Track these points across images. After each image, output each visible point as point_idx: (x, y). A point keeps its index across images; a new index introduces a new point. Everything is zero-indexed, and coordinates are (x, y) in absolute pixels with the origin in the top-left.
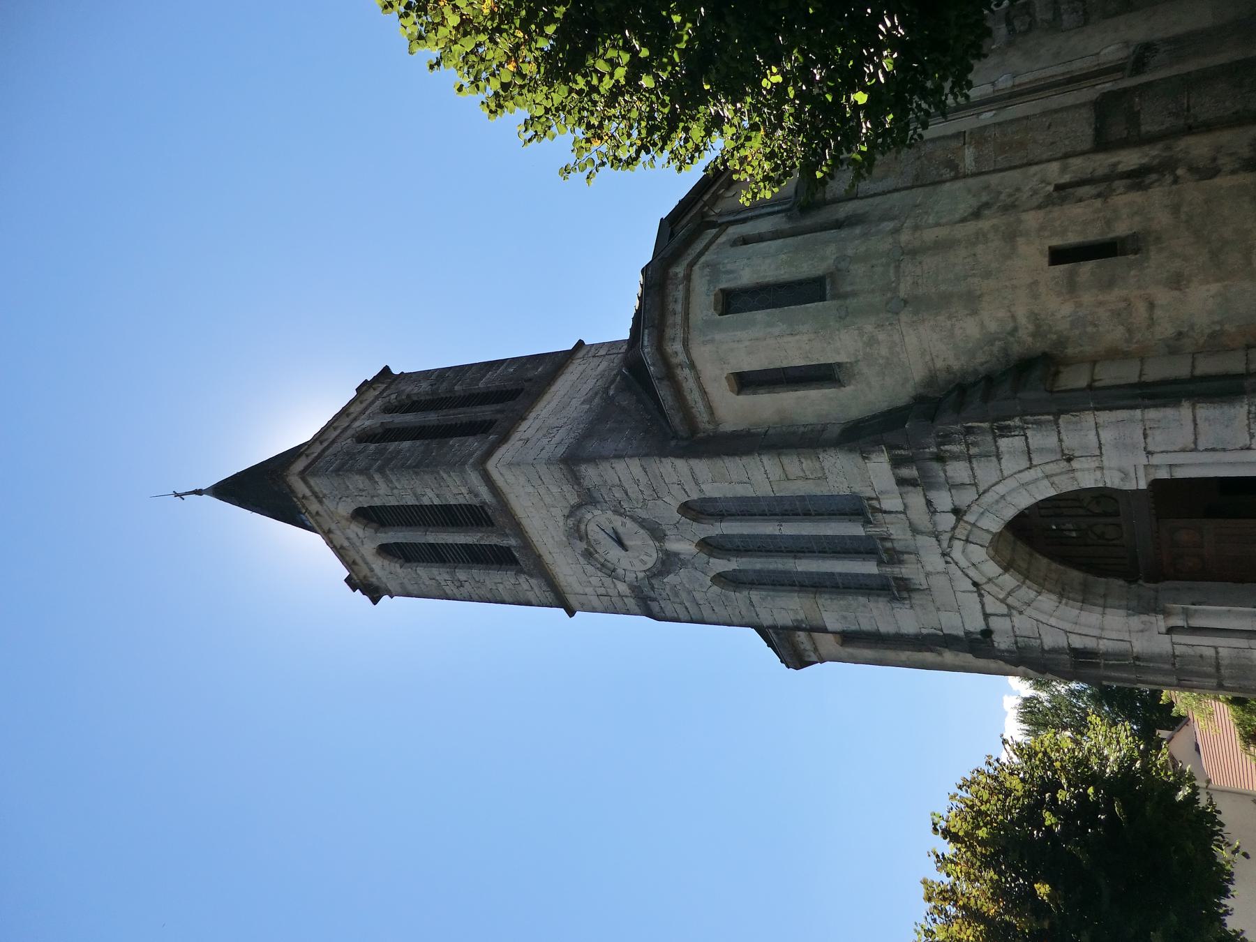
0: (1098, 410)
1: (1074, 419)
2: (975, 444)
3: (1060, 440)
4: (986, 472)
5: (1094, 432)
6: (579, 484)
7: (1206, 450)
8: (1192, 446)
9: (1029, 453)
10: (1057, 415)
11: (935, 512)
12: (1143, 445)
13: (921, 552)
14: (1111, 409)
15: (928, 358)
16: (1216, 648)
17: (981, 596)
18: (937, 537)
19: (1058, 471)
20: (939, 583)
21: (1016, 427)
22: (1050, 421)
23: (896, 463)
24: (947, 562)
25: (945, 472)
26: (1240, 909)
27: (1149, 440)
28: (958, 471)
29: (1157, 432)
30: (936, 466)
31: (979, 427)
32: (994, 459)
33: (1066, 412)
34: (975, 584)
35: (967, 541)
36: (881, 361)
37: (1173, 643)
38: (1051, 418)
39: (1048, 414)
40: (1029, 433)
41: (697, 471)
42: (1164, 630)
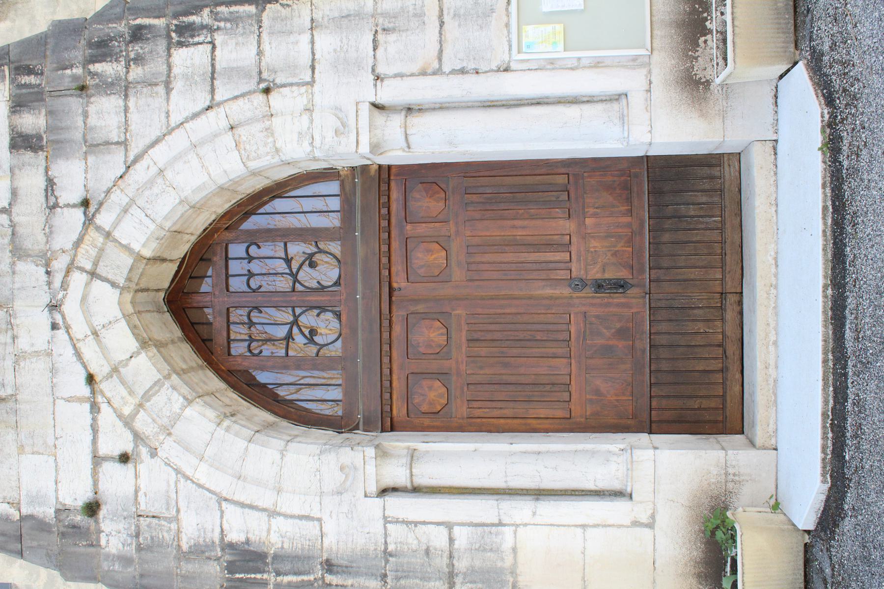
3: (260, 53)
4: (146, 114)
5: (306, 37)
6: (29, 256)
7: (453, 72)
8: (436, 65)
9: (213, 78)
12: (371, 62)
13: (18, 305)
16: (449, 526)
17: (95, 408)
21: (203, 27)
22: (250, 16)
25: (86, 115)
27: (380, 52)
28: (104, 113)
29: (392, 37)
30: (75, 103)
32: (161, 89)
37: (386, 520)
40: (219, 38)
41: (170, 265)
42: (373, 489)
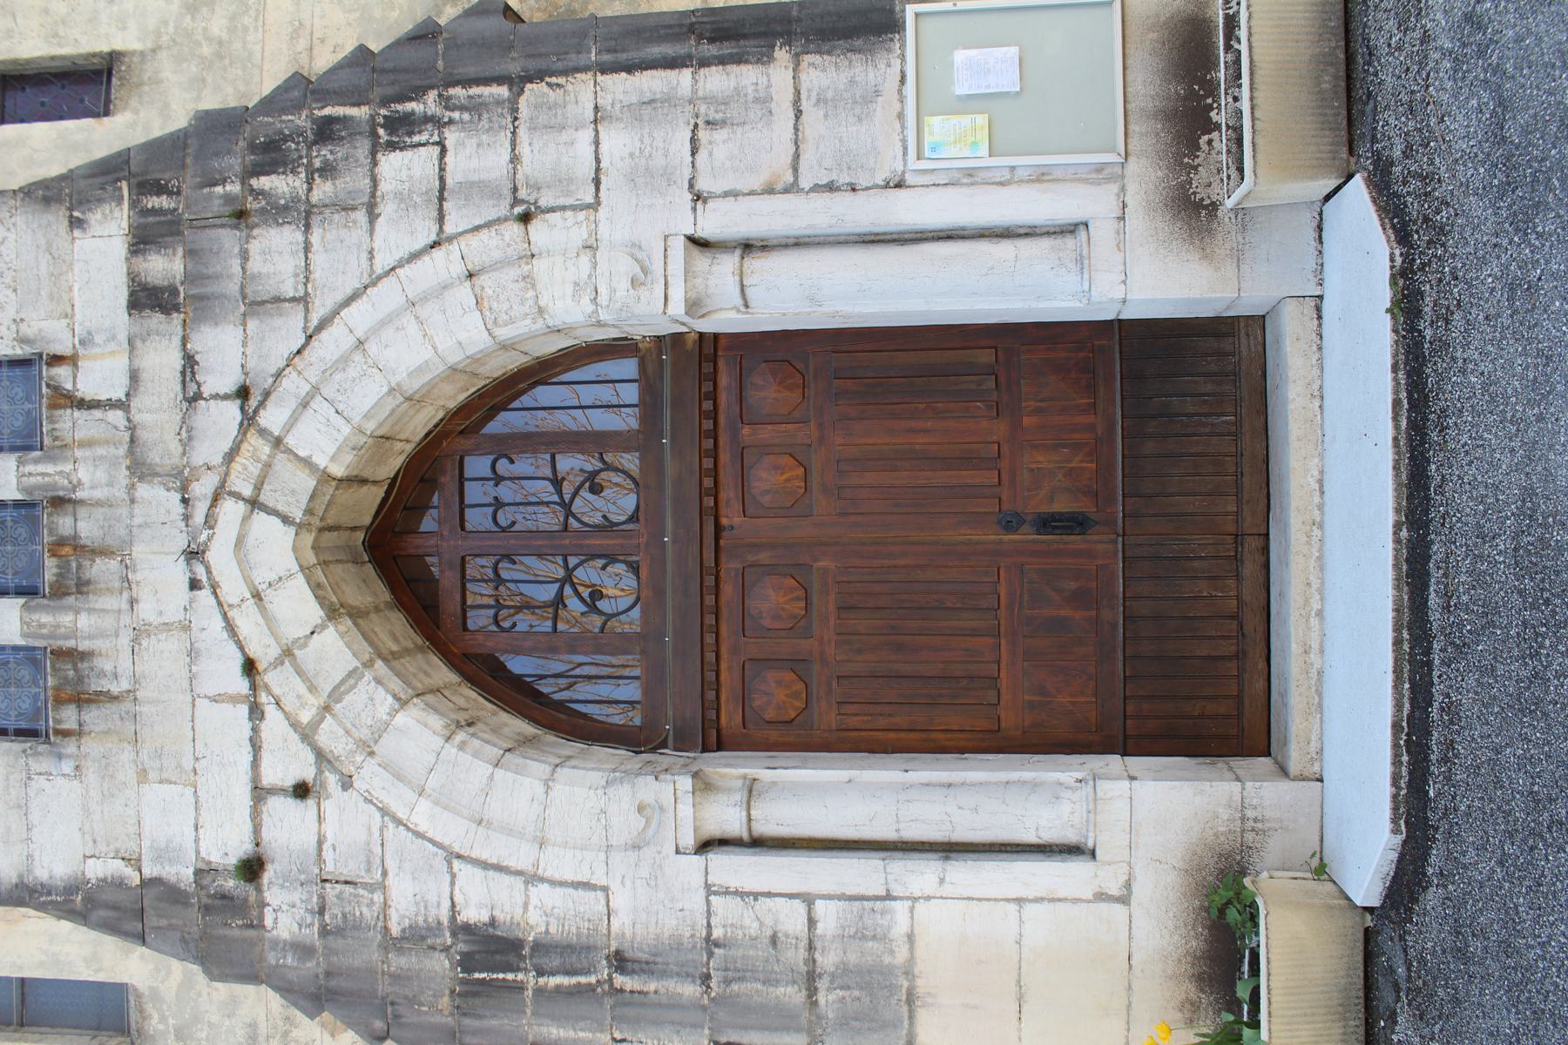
0: (605, 69)
1: (553, 95)
2: (328, 170)
3: (515, 159)
4: (337, 255)
7: (816, 188)
9: (441, 199)
10: (517, 83)
11: (198, 396)
13: (139, 551)
14: (630, 68)
15: (302, 44)
16: (808, 900)
17: (256, 712)
18: (183, 484)
19: (497, 255)
20: (162, 661)
22: (499, 102)
23: (142, 240)
24: (194, 585)
25: (245, 256)
26: (928, 1027)
27: (702, 157)
29: (721, 135)
30: (228, 238)
31: (344, 120)
32: (361, 216)
33: (538, 76)
34: (250, 667)
35: (254, 504)
36: (206, 50)
37: (709, 890)
38: (503, 91)
39: (499, 80)
42: (689, 841)
